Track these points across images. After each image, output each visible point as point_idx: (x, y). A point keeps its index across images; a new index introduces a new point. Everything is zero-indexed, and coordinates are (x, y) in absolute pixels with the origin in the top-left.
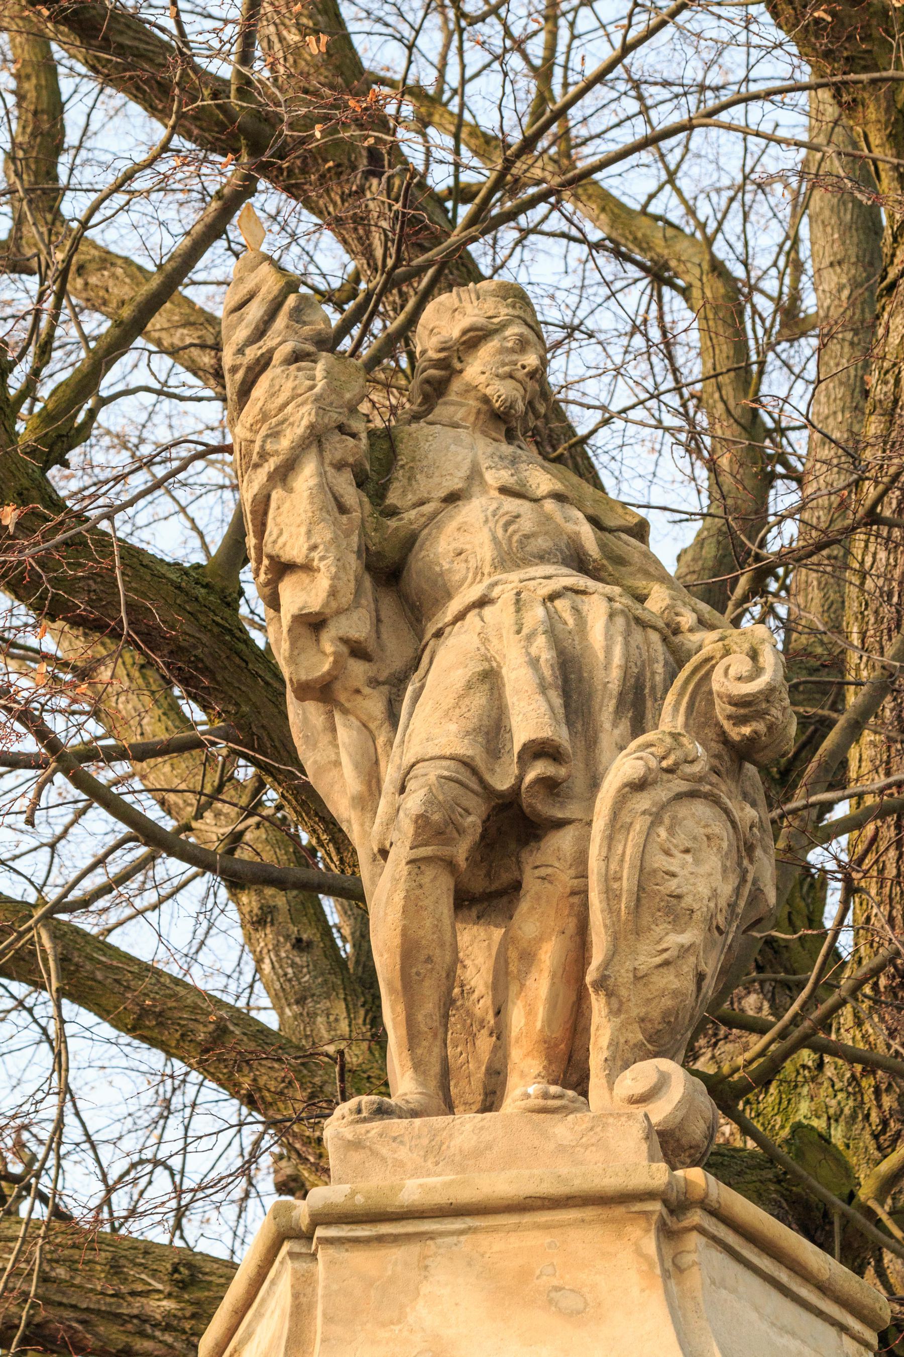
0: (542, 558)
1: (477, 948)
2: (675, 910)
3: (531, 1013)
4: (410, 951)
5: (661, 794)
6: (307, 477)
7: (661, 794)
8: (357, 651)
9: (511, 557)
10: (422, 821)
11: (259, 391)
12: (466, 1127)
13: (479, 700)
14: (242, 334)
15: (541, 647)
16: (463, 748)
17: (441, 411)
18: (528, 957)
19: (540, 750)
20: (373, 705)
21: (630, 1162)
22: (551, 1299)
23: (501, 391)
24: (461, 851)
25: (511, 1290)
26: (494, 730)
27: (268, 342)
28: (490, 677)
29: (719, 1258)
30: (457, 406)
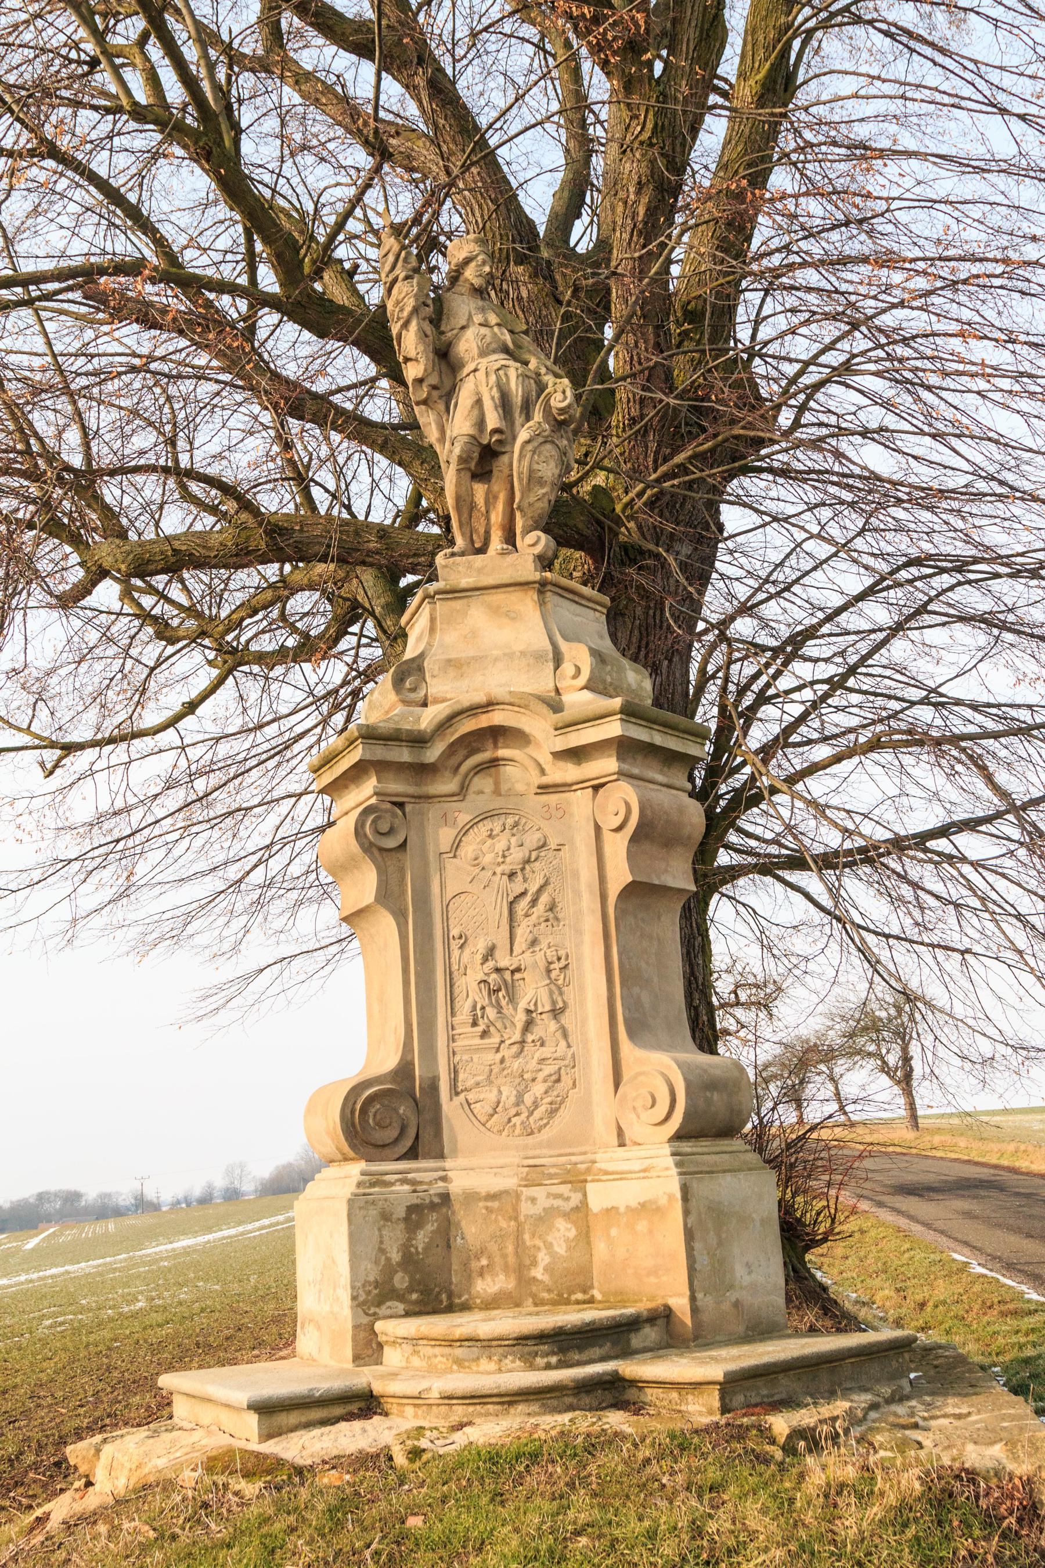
0: (494, 352)
1: (480, 490)
2: (541, 482)
3: (497, 516)
4: (458, 499)
5: (535, 444)
6: (414, 326)
7: (535, 444)
8: (434, 387)
9: (483, 353)
10: (460, 458)
11: (395, 291)
12: (479, 560)
13: (476, 412)
14: (387, 268)
15: (497, 395)
16: (471, 432)
17: (457, 289)
18: (496, 498)
19: (496, 431)
20: (441, 407)
21: (529, 571)
22: (507, 615)
23: (477, 282)
24: (473, 465)
25: (495, 611)
26: (481, 423)
27: (397, 271)
28: (479, 402)
29: (556, 598)
30: (462, 287)
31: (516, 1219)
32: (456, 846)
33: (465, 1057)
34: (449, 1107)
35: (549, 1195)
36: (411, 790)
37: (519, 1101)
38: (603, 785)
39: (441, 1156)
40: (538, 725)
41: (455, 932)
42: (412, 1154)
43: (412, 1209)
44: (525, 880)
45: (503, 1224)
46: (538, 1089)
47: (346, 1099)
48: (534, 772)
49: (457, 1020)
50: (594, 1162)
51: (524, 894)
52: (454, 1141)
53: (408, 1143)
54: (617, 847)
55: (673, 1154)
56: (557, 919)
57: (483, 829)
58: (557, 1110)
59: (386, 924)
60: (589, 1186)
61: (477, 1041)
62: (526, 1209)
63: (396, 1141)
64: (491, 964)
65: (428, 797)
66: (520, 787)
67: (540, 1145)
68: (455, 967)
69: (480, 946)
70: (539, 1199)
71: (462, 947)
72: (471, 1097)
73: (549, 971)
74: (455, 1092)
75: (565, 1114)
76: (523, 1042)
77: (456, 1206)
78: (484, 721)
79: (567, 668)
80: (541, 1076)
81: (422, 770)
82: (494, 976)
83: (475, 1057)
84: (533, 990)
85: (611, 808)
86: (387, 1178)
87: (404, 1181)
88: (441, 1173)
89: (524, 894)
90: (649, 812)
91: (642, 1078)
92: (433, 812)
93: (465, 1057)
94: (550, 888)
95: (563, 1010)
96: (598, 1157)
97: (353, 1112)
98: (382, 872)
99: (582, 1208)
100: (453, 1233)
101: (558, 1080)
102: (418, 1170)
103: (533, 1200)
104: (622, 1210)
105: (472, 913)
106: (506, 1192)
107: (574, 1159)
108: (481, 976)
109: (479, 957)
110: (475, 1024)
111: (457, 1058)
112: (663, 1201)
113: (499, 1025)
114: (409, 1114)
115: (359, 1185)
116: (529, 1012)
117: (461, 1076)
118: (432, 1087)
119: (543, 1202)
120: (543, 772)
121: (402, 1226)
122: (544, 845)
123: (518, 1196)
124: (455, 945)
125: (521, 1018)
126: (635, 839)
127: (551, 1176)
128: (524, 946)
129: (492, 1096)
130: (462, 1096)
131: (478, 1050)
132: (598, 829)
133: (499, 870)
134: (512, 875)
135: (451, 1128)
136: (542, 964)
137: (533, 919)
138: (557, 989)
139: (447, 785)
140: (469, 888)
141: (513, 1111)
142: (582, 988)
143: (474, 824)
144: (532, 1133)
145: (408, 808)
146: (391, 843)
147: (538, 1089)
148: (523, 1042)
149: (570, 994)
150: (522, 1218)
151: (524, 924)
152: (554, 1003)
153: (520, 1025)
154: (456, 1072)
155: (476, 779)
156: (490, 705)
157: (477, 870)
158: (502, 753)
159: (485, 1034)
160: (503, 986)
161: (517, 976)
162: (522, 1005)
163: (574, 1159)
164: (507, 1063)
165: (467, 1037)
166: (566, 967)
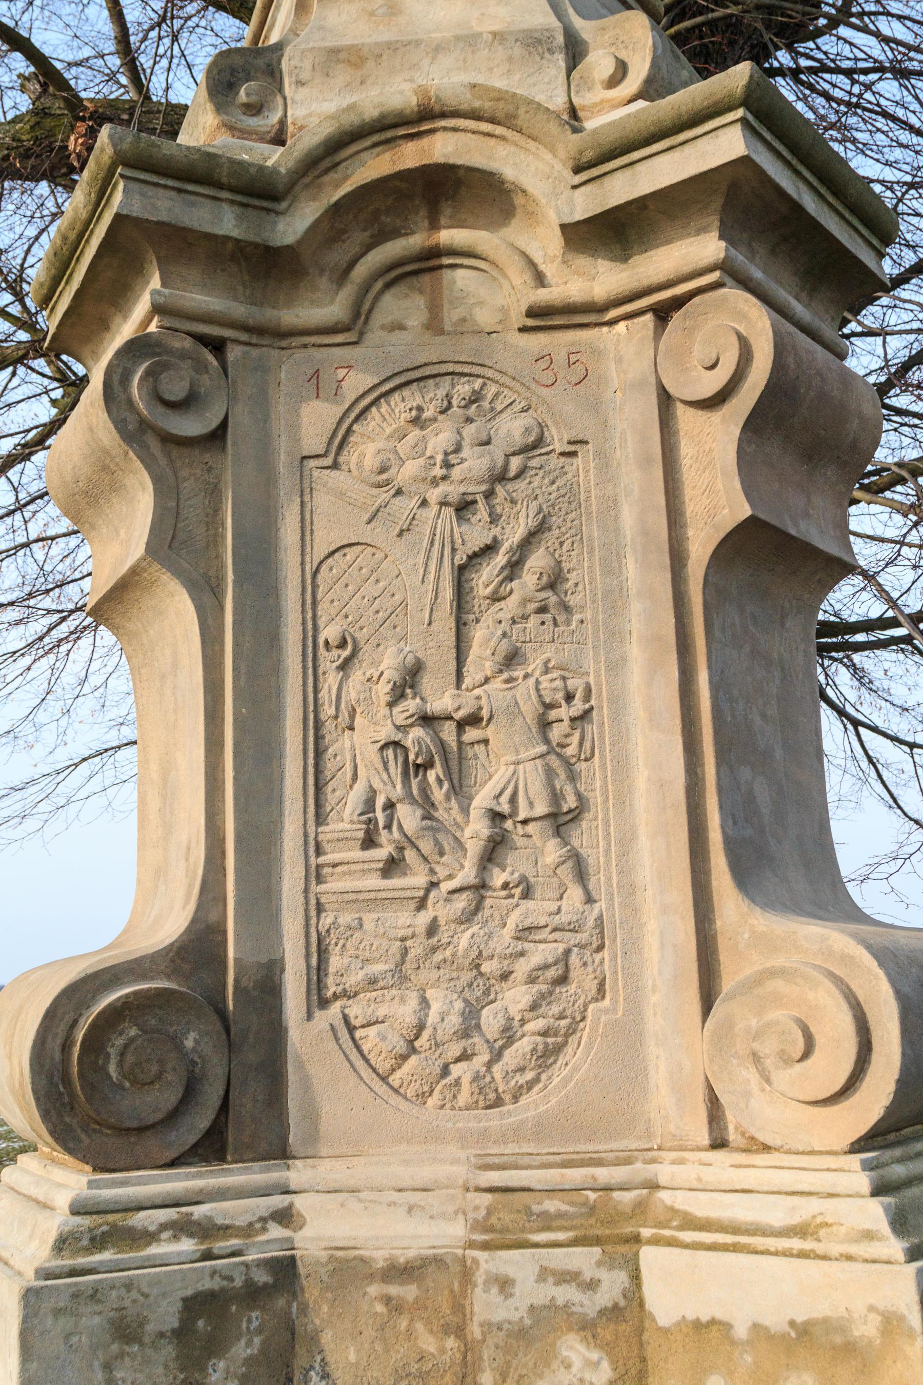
31: (460, 1331)
32: (340, 441)
33: (346, 918)
34: (305, 1035)
35: (544, 1274)
36: (239, 310)
37: (470, 1025)
38: (679, 303)
39: (281, 1153)
40: (537, 171)
41: (330, 632)
42: (212, 1148)
43: (199, 1305)
44: (494, 519)
45: (428, 1343)
46: (516, 998)
47: (50, 1016)
48: (519, 277)
49: (329, 831)
50: (654, 1186)
51: (490, 549)
52: (312, 1117)
53: (201, 1120)
54: (712, 446)
55: (878, 1190)
56: (566, 608)
57: (400, 407)
58: (558, 1049)
59: (174, 611)
60: (649, 1256)
61: (375, 881)
62: (486, 1307)
63: (174, 1116)
64: (411, 705)
65: (281, 335)
66: (484, 318)
67: (517, 1133)
68: (328, 711)
69: (388, 663)
70: (522, 1279)
71: (345, 666)
72: (357, 1011)
73: (545, 725)
74: (318, 996)
75: (576, 1060)
76: (481, 887)
77: (311, 1292)
78: (410, 156)
79: (599, 63)
80: (522, 968)
81: (270, 267)
82: (418, 732)
83: (369, 920)
84: (505, 768)
85: (700, 352)
86: (141, 1219)
87: (182, 1228)
88: (278, 1201)
89: (490, 549)
90: (790, 361)
91: (778, 985)
92: (288, 368)
93: (346, 918)
94: (550, 539)
95: (576, 815)
96: (664, 1172)
97: (66, 1047)
98: (166, 491)
99: (630, 1310)
100: (300, 1361)
101: (563, 979)
102: (221, 1194)
103: (505, 1285)
104: (741, 1331)
105: (371, 590)
106: (438, 1261)
107: (603, 1174)
108: (386, 732)
109: (383, 689)
110: (369, 842)
111: (327, 920)
112: (867, 1329)
113: (426, 846)
114: (207, 1049)
115: (62, 1244)
116: (496, 817)
117: (335, 962)
118: (266, 987)
119: (531, 1292)
120: (540, 279)
121: (169, 1351)
122: (536, 445)
123: (466, 1273)
124: (329, 661)
125: (476, 830)
126: (756, 425)
127: (547, 1222)
128: (489, 667)
129: (405, 1011)
130: (335, 1008)
131: (376, 902)
132: (665, 400)
133: (434, 495)
134: (464, 507)
135: (306, 1085)
136: (530, 708)
137: (511, 606)
138: (562, 765)
139: (324, 307)
140: (365, 534)
141: (455, 1050)
142: (622, 765)
143: (379, 395)
144: (498, 1102)
145: (233, 353)
146: (190, 426)
147: (516, 998)
148: (481, 887)
149: (595, 779)
150: (475, 1331)
151: (487, 620)
152: (556, 797)
153: (474, 848)
154: (323, 952)
155: (388, 299)
156: (426, 117)
157: (384, 495)
158: (448, 236)
159: (392, 866)
160: (437, 755)
161: (471, 734)
162: (482, 800)
163: (603, 1174)
164: (443, 936)
165: (354, 874)
166: (586, 715)
